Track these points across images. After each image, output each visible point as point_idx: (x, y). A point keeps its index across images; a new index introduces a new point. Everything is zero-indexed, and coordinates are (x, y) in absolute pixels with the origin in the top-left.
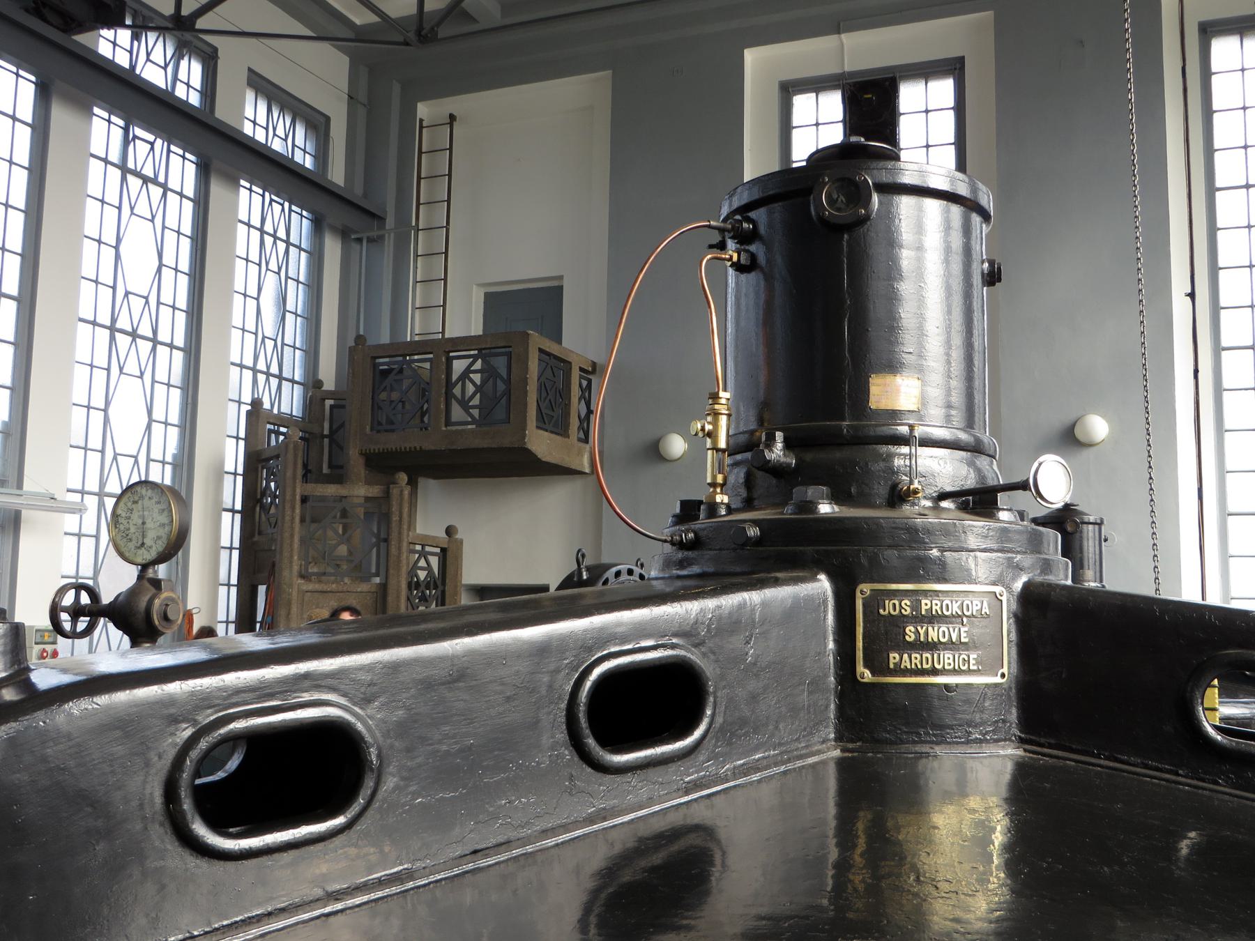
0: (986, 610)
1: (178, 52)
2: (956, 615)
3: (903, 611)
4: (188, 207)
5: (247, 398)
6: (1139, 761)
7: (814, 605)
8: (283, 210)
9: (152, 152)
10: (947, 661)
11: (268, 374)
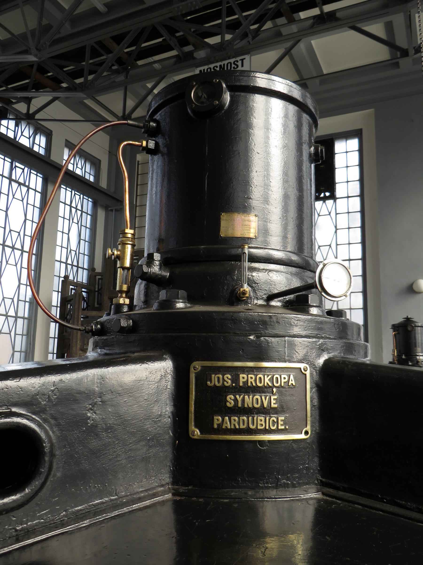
0: (292, 382)
1: (35, 132)
2: (268, 386)
3: (225, 383)
4: (38, 196)
5: (63, 275)
6: (414, 506)
8: (80, 198)
9: (23, 173)
10: (259, 422)
11: (72, 265)
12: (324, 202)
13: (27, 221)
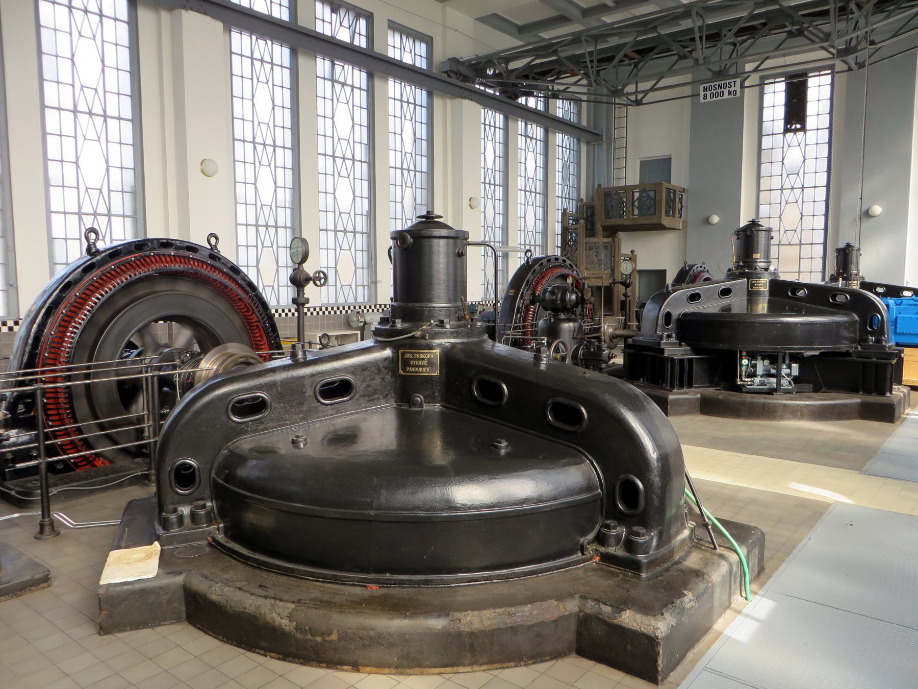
7: (745, 281)
12: (795, 134)
13: (276, 108)
